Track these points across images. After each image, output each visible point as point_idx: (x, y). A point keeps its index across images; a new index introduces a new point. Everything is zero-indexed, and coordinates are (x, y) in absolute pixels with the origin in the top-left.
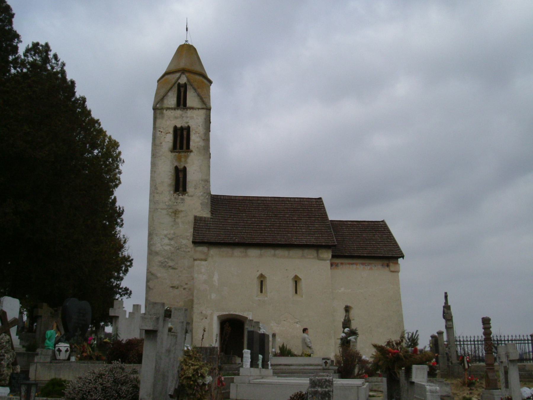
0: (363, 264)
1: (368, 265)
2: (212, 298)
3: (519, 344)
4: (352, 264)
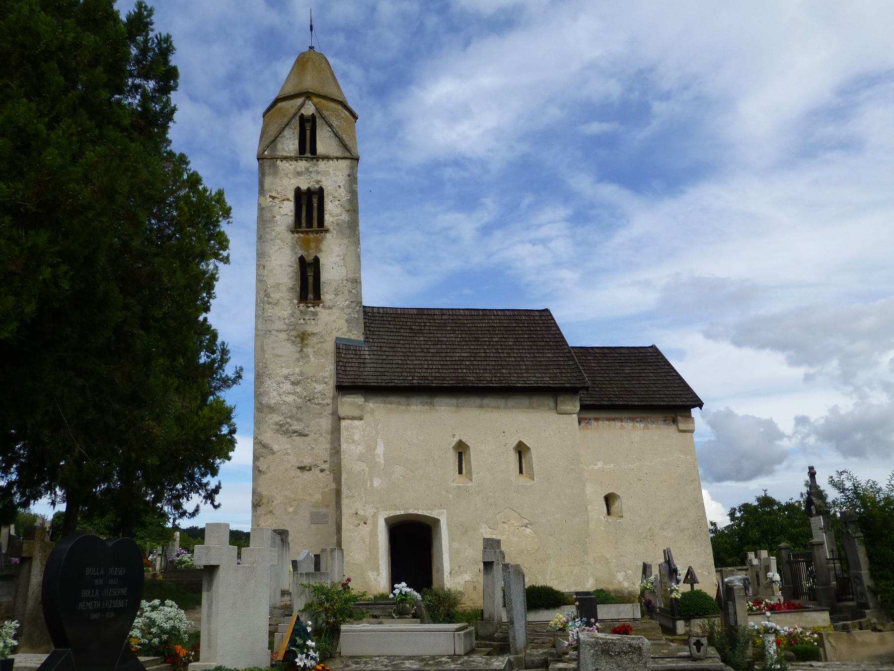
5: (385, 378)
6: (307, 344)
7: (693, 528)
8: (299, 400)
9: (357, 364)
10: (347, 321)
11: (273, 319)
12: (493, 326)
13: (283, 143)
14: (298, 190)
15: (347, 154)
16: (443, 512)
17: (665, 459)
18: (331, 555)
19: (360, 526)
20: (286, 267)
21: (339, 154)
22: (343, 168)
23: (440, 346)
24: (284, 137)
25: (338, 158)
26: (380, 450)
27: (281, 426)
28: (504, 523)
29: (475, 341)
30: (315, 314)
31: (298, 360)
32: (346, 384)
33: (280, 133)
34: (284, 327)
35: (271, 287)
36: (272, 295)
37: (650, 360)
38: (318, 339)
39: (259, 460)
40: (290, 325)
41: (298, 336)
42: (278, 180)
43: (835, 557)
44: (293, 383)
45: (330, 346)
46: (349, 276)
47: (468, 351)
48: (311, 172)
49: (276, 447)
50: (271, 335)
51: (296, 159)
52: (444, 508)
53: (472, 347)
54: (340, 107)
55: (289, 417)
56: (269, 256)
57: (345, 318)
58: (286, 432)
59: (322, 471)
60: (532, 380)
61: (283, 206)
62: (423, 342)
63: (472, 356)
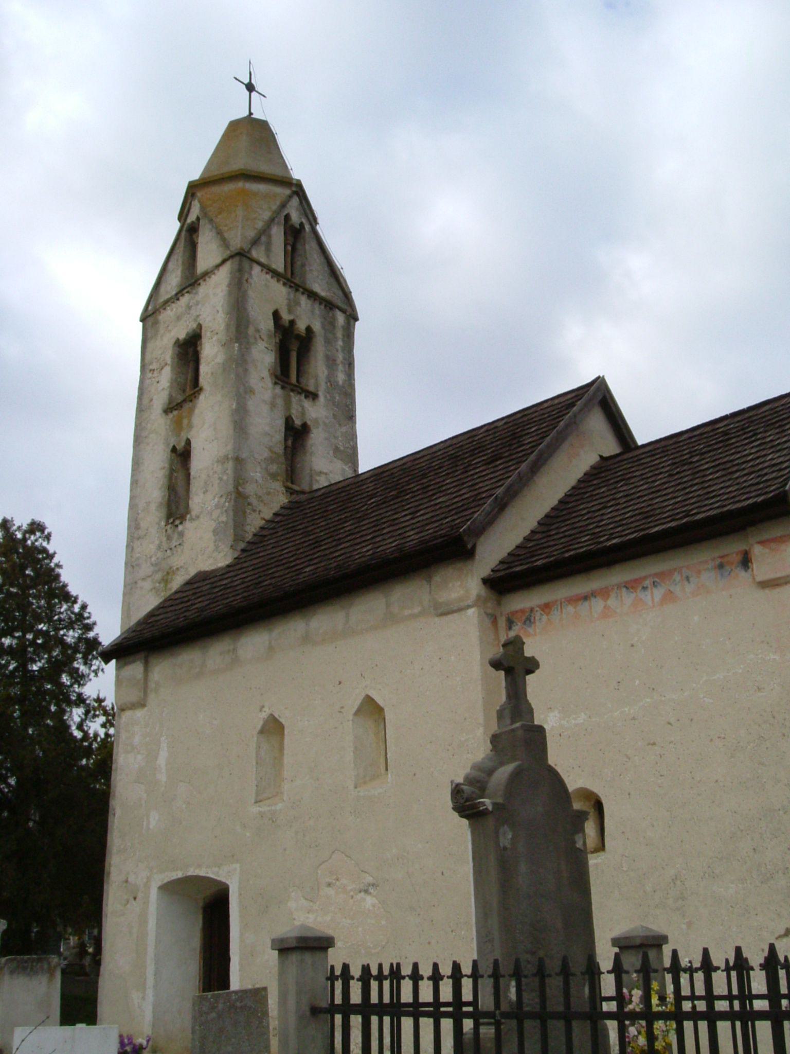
0: (630, 586)
1: (654, 584)
2: (151, 827)
3: (556, 1028)
4: (586, 598)
16: (235, 869)
28: (329, 885)
43: (561, 1024)
54: (240, 184)
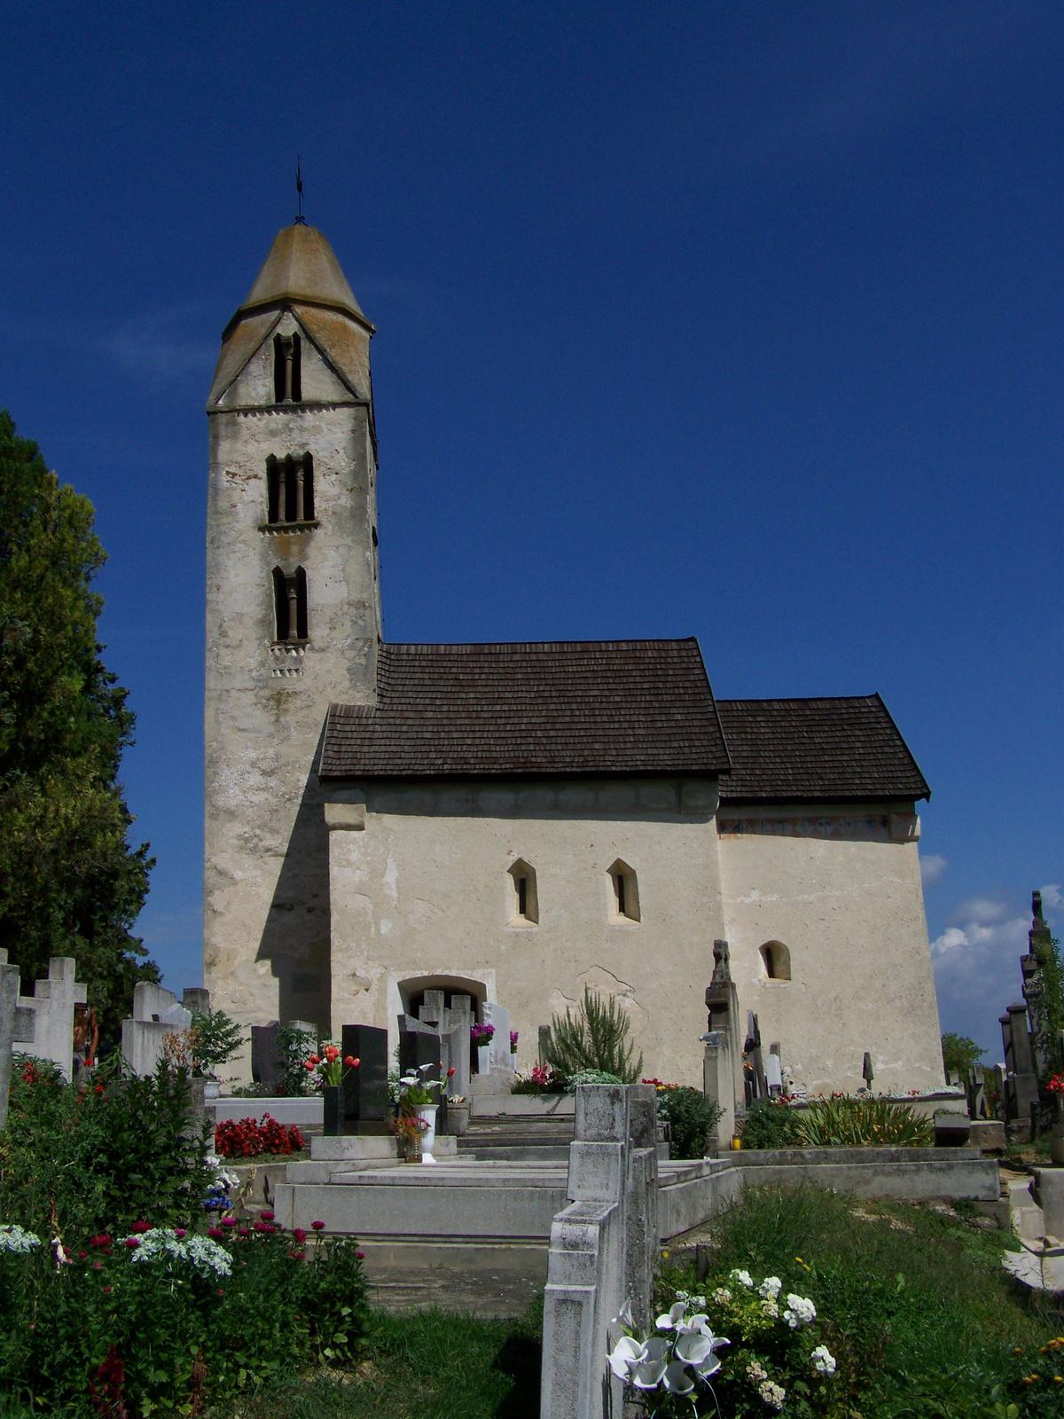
5: (399, 762)
6: (286, 711)
7: (909, 997)
8: (274, 800)
9: (359, 742)
10: (349, 670)
11: (233, 671)
12: (594, 670)
13: (247, 384)
14: (272, 462)
15: (349, 397)
16: (491, 973)
17: (866, 886)
18: (1041, 1239)
19: (359, 994)
20: (252, 588)
21: (335, 398)
22: (343, 420)
23: (498, 708)
24: (250, 374)
25: (335, 405)
26: (391, 877)
27: (247, 840)
29: (559, 697)
30: (299, 660)
31: (271, 736)
32: (335, 774)
33: (243, 369)
34: (251, 684)
35: (229, 620)
36: (231, 633)
37: (863, 720)
38: (303, 701)
39: (213, 894)
40: (260, 681)
41: (272, 697)
42: (239, 445)
44: (264, 773)
45: (320, 715)
46: (352, 598)
47: (544, 713)
48: (291, 430)
49: (238, 875)
50: (230, 697)
51: (268, 409)
52: (492, 967)
53: (552, 707)
54: (340, 318)
55: (259, 827)
56: (225, 570)
57: (346, 666)
58: (254, 850)
59: (310, 910)
60: (638, 759)
61: (246, 487)
62: (472, 702)
63: (548, 723)
